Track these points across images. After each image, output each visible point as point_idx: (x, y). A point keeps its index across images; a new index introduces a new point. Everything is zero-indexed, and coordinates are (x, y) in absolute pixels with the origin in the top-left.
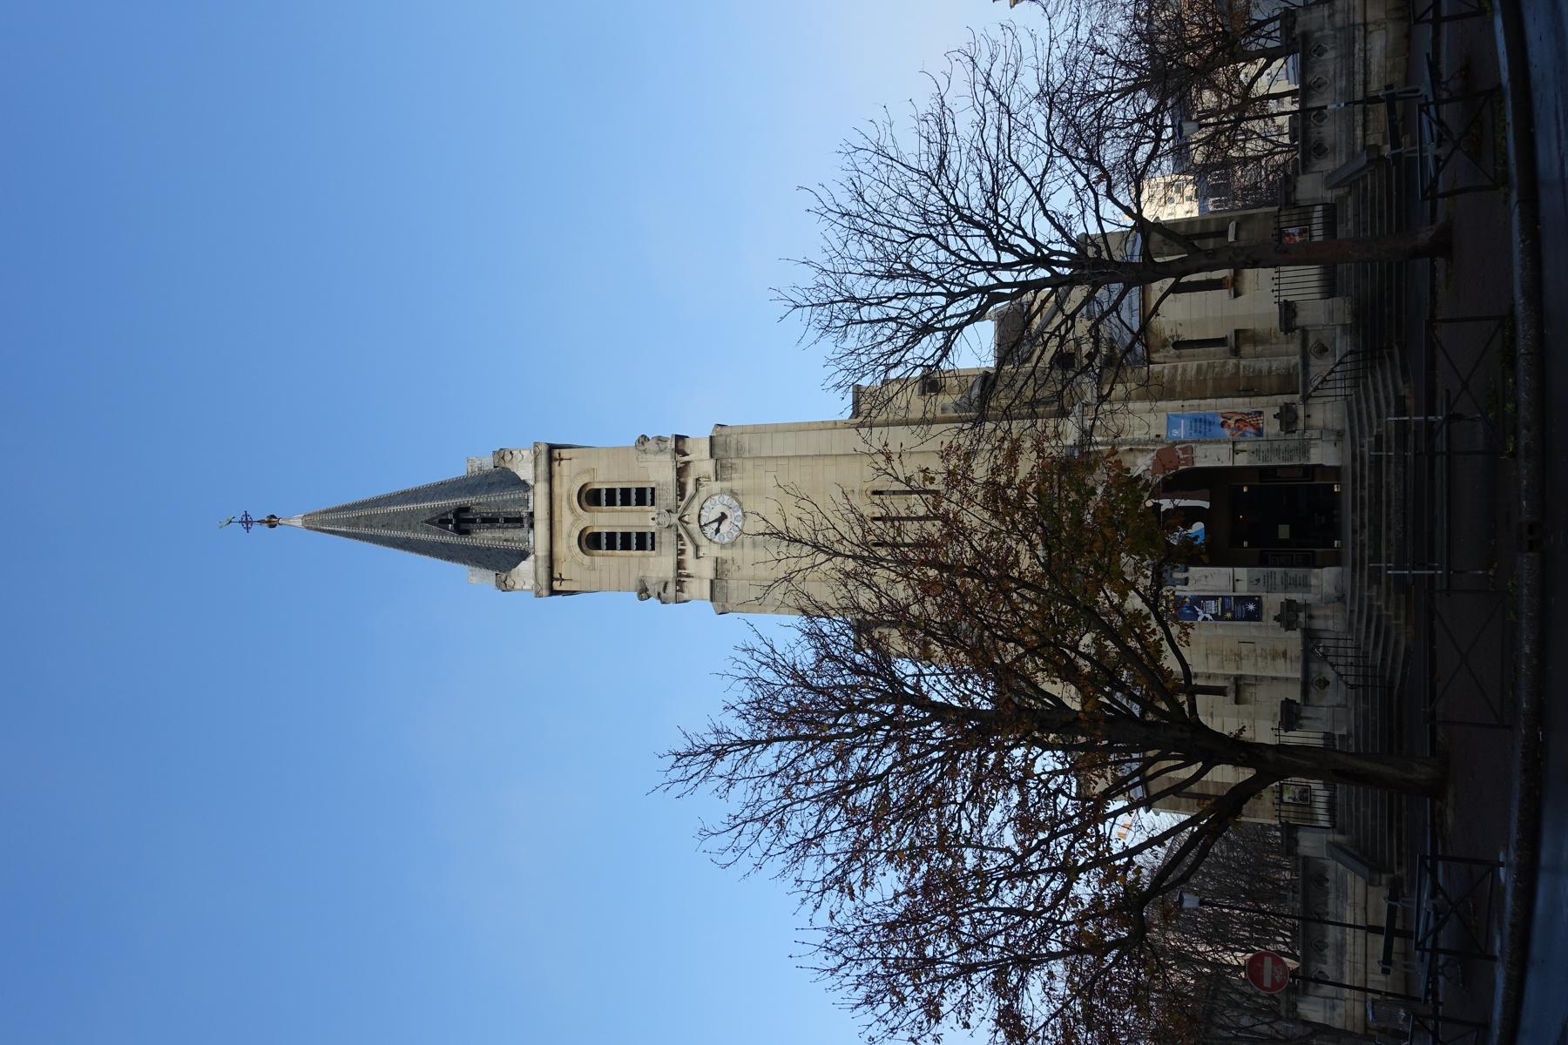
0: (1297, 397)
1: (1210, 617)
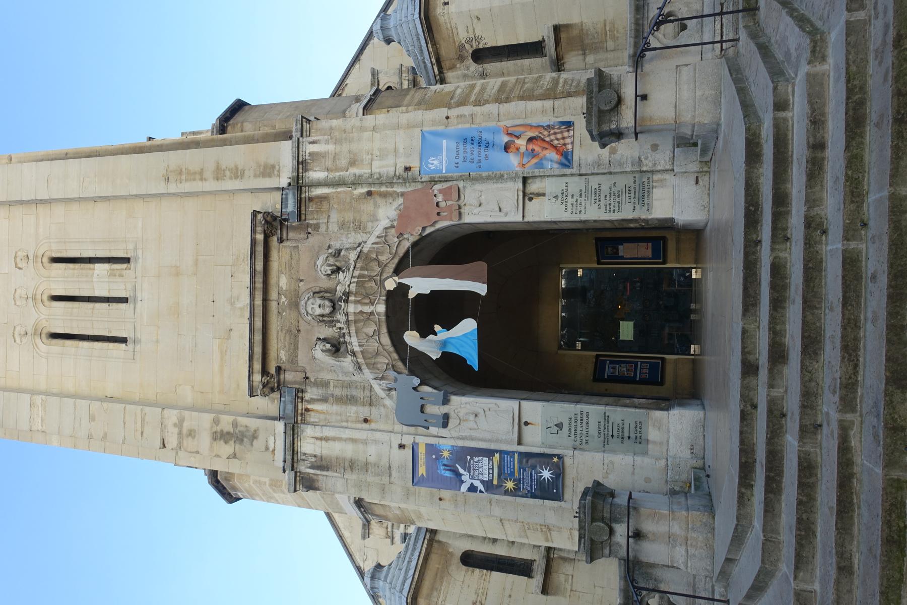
1: (481, 487)
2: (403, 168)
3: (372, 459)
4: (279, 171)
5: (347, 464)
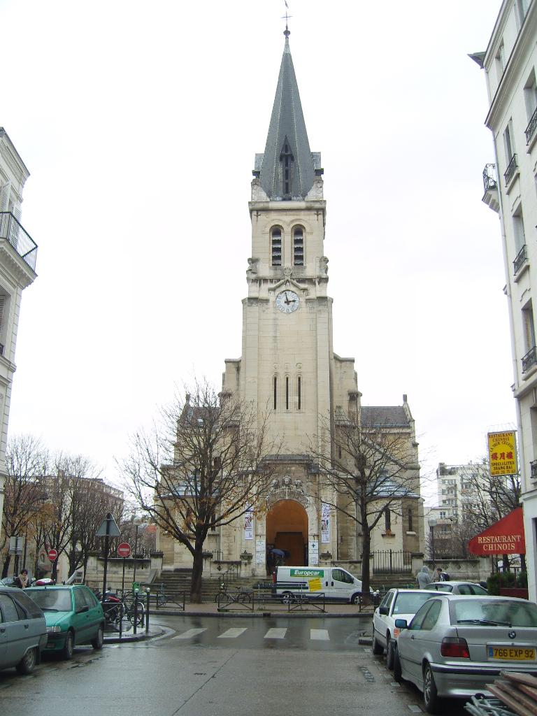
0: (336, 560)
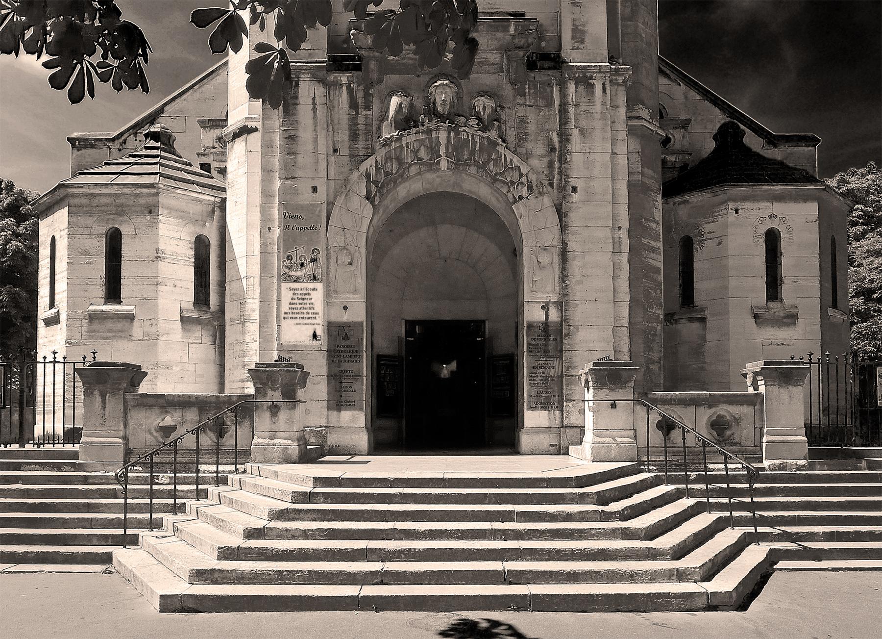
2: (575, 185)
3: (300, 158)
4: (578, 48)
5: (293, 133)
